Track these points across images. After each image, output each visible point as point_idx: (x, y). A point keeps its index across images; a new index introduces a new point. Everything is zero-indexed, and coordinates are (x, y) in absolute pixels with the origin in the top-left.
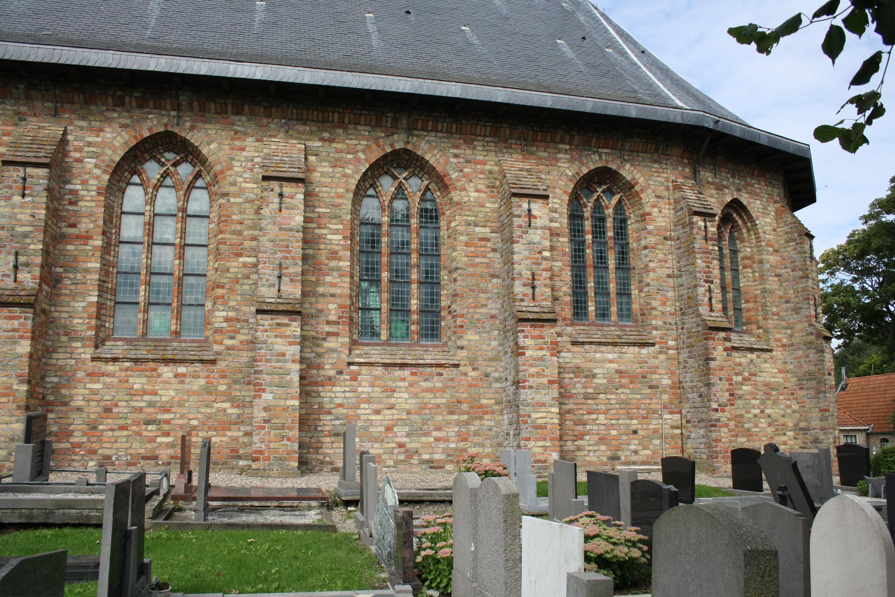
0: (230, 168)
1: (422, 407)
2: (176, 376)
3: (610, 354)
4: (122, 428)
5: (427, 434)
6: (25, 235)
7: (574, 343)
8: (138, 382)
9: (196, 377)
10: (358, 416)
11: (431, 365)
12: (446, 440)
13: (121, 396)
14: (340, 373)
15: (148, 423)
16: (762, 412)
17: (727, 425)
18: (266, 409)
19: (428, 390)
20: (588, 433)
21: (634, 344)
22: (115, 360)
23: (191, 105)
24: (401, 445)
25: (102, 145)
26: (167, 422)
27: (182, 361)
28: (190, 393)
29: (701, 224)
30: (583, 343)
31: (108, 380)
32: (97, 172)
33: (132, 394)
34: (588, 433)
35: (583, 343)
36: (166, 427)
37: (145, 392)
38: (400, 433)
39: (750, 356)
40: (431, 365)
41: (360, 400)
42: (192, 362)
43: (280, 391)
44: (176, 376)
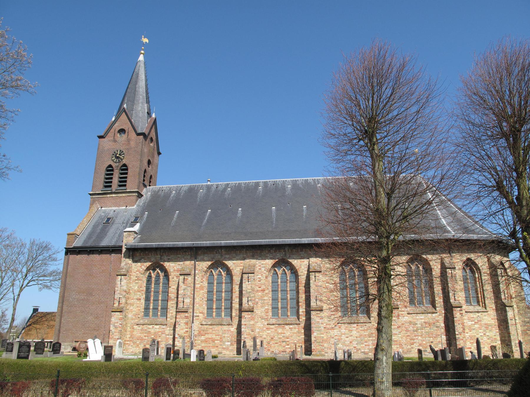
0: (301, 267)
1: (361, 336)
2: (290, 328)
3: (422, 316)
4: (276, 343)
5: (362, 344)
6: (250, 292)
7: (408, 314)
8: (280, 330)
9: (295, 328)
10: (341, 339)
11: (363, 323)
12: (369, 345)
13: (276, 334)
14: (336, 326)
15: (283, 342)
16: (484, 334)
17: (462, 340)
18: (315, 337)
19: (363, 330)
20: (415, 343)
21: (430, 313)
22: (273, 324)
23: (288, 250)
24: (355, 347)
25: (266, 264)
26: (288, 341)
27: (291, 324)
28: (294, 333)
29: (450, 271)
30: (412, 314)
31: (272, 330)
32: (265, 272)
33: (278, 334)
34: (415, 343)
35: (412, 314)
36: (288, 343)
37: (281, 333)
38: (355, 343)
39: (477, 314)
40: (363, 323)
41: (342, 334)
42: (294, 324)
43: (319, 332)
44: (290, 328)
